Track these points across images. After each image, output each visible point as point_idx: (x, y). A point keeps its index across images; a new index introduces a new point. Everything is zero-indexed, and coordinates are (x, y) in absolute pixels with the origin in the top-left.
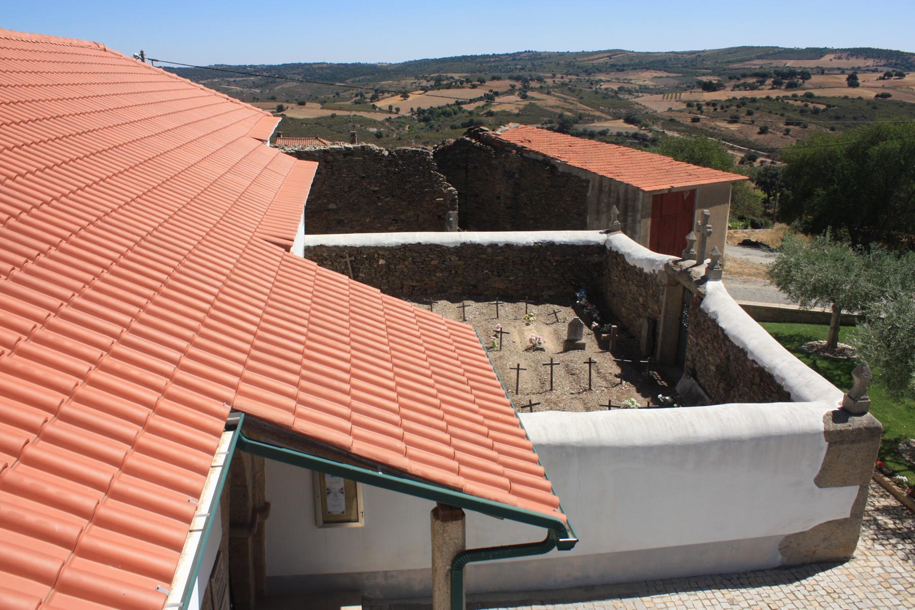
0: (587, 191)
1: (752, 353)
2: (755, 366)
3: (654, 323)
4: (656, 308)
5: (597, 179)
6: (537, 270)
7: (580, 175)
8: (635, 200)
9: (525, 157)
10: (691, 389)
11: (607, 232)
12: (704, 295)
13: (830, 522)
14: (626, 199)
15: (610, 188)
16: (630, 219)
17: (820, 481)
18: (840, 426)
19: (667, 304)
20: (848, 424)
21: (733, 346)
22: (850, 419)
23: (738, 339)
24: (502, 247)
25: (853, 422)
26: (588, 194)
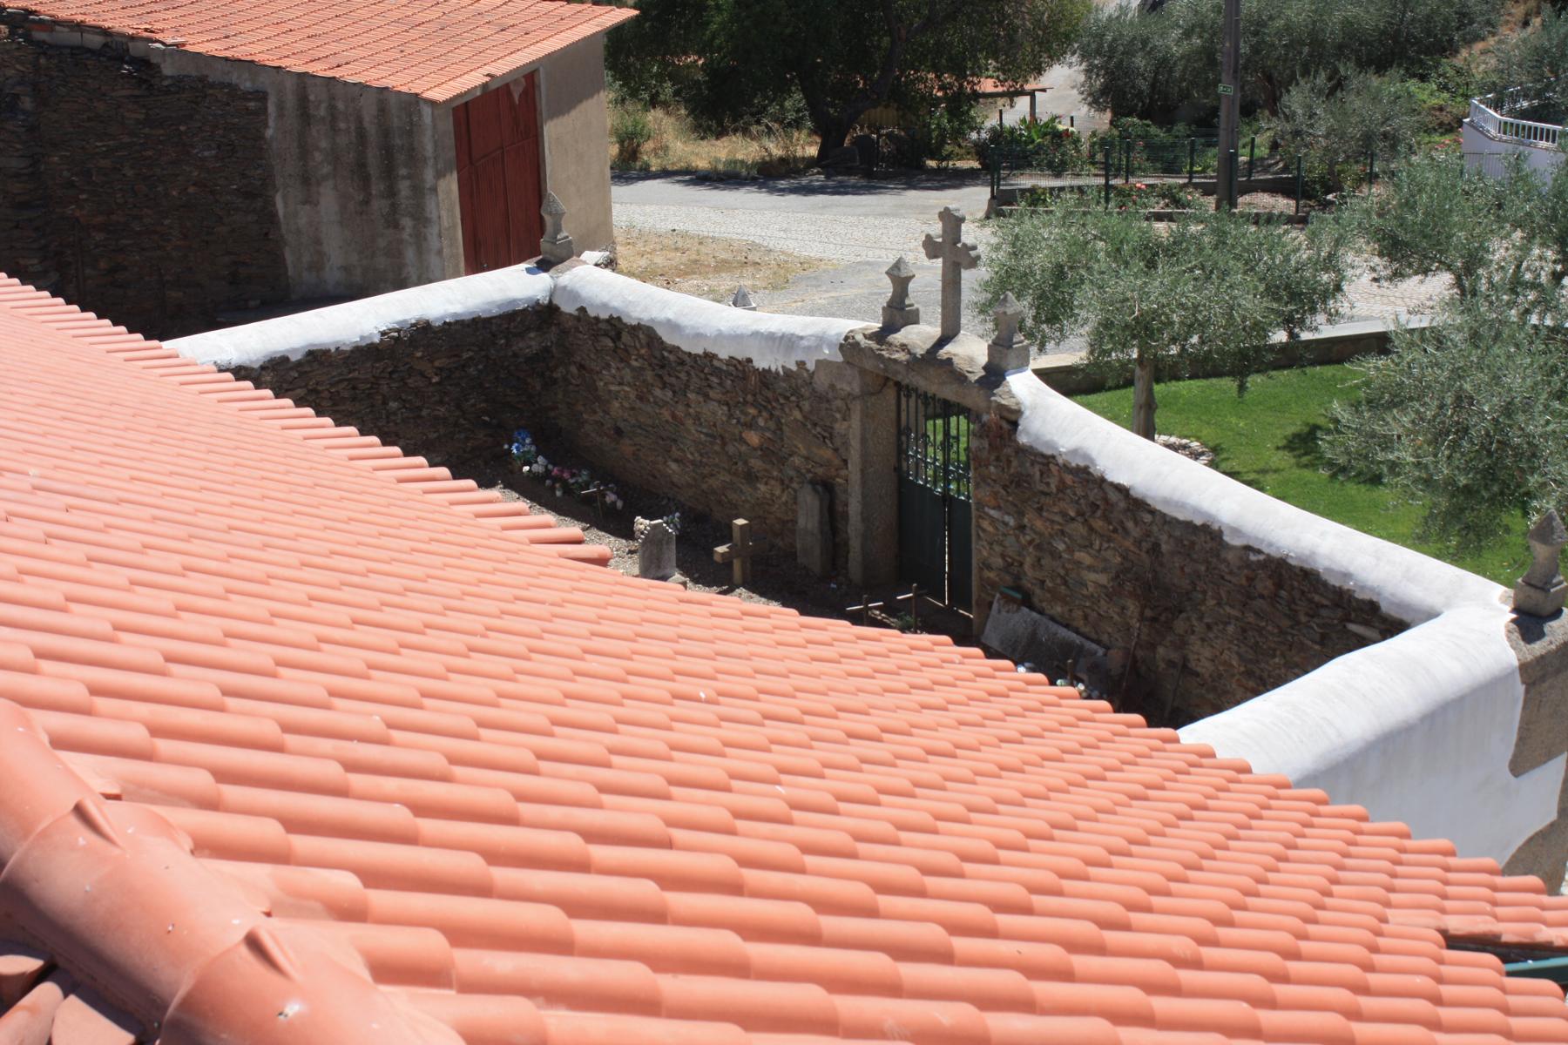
0: (266, 126)
1: (1236, 531)
2: (1253, 558)
3: (827, 489)
4: (827, 453)
5: (289, 84)
6: (393, 405)
7: (234, 79)
8: (412, 130)
9: (40, 44)
10: (1033, 635)
11: (544, 266)
12: (1019, 412)
13: (1531, 839)
14: (386, 133)
15: (332, 108)
16: (404, 187)
17: (1519, 766)
18: (1539, 648)
19: (863, 441)
20: (1547, 639)
21: (1167, 521)
22: (1547, 627)
23: (1182, 506)
24: (299, 364)
25: (1553, 632)
26: (269, 133)
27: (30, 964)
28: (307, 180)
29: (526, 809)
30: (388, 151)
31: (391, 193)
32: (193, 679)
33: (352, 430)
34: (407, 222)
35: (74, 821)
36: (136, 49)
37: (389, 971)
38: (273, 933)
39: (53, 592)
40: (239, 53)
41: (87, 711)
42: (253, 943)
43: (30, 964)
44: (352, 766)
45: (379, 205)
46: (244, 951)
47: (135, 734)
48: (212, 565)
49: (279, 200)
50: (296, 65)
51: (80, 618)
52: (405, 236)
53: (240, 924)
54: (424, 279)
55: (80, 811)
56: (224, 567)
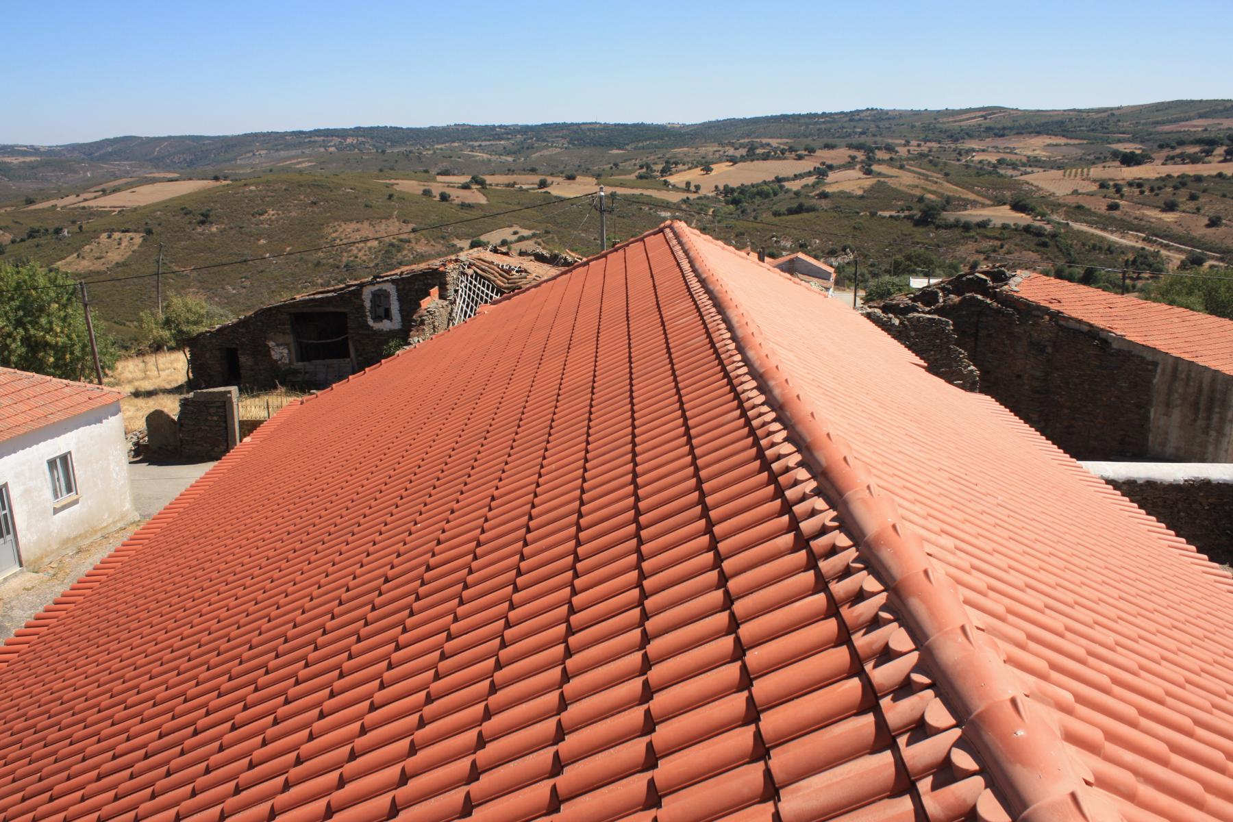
5: (1170, 361)
6: (1182, 514)
7: (1144, 354)
9: (1061, 326)
14: (1213, 391)
15: (1188, 376)
16: (1216, 417)
26: (1155, 381)
27: (926, 680)
28: (1168, 405)
29: (1169, 700)
30: (1211, 400)
31: (1209, 418)
32: (1054, 618)
33: (1172, 532)
34: (1213, 434)
35: (959, 631)
36: (1102, 335)
37: (1071, 738)
38: (1085, 794)
39: (988, 546)
40: (1150, 344)
41: (985, 595)
42: (1014, 702)
43: (926, 680)
44: (1090, 653)
45: (1201, 423)
46: (1009, 704)
47: (1000, 609)
48: (1063, 556)
49: (1152, 411)
50: (1175, 353)
51: (1012, 577)
52: (1211, 440)
53: (1011, 693)
54: (1215, 459)
55: (963, 628)
56: (1115, 603)
